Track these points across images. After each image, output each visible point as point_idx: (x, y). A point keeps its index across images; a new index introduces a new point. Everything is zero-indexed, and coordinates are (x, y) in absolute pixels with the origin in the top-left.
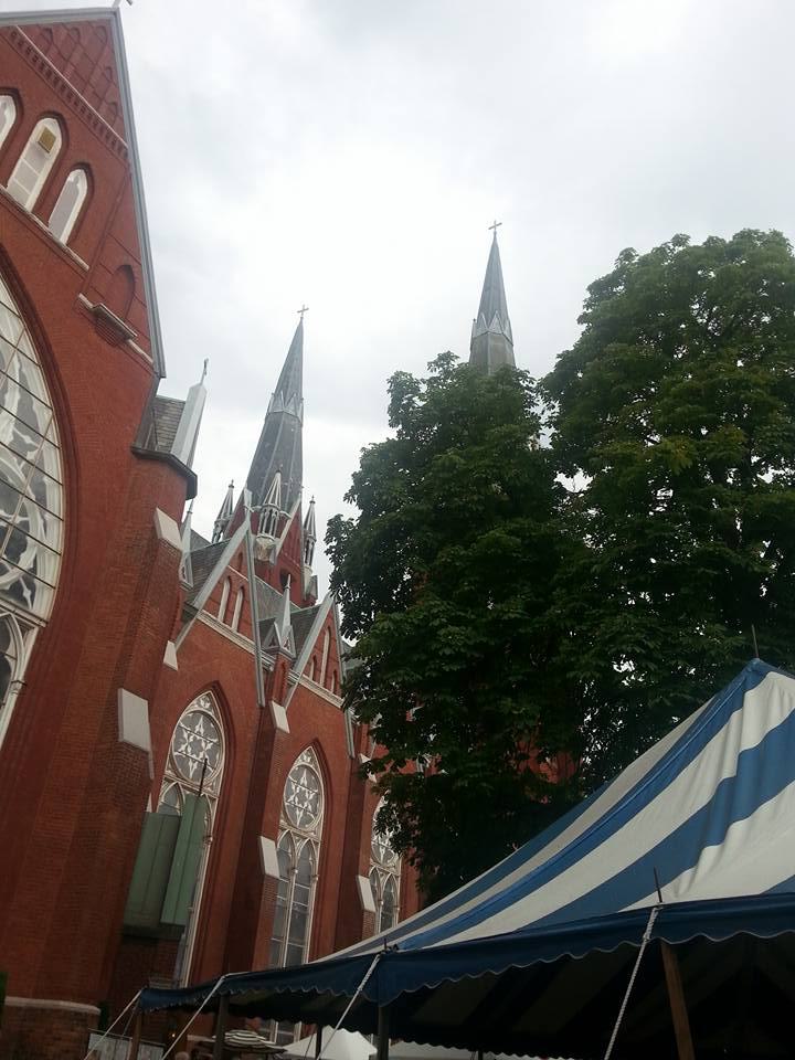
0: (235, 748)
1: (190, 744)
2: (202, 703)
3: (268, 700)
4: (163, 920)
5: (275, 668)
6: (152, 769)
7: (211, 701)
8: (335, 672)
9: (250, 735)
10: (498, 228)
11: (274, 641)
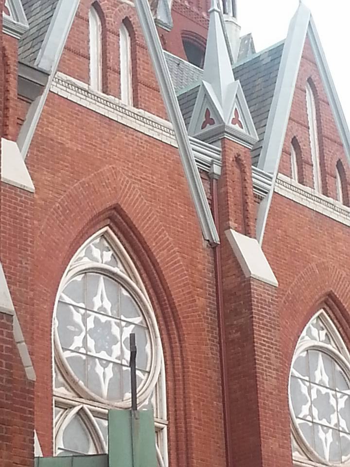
0: (178, 328)
1: (90, 332)
2: (96, 253)
3: (222, 228)
5: (223, 166)
6: (26, 359)
7: (112, 246)
8: (339, 165)
9: (201, 302)
11: (210, 116)
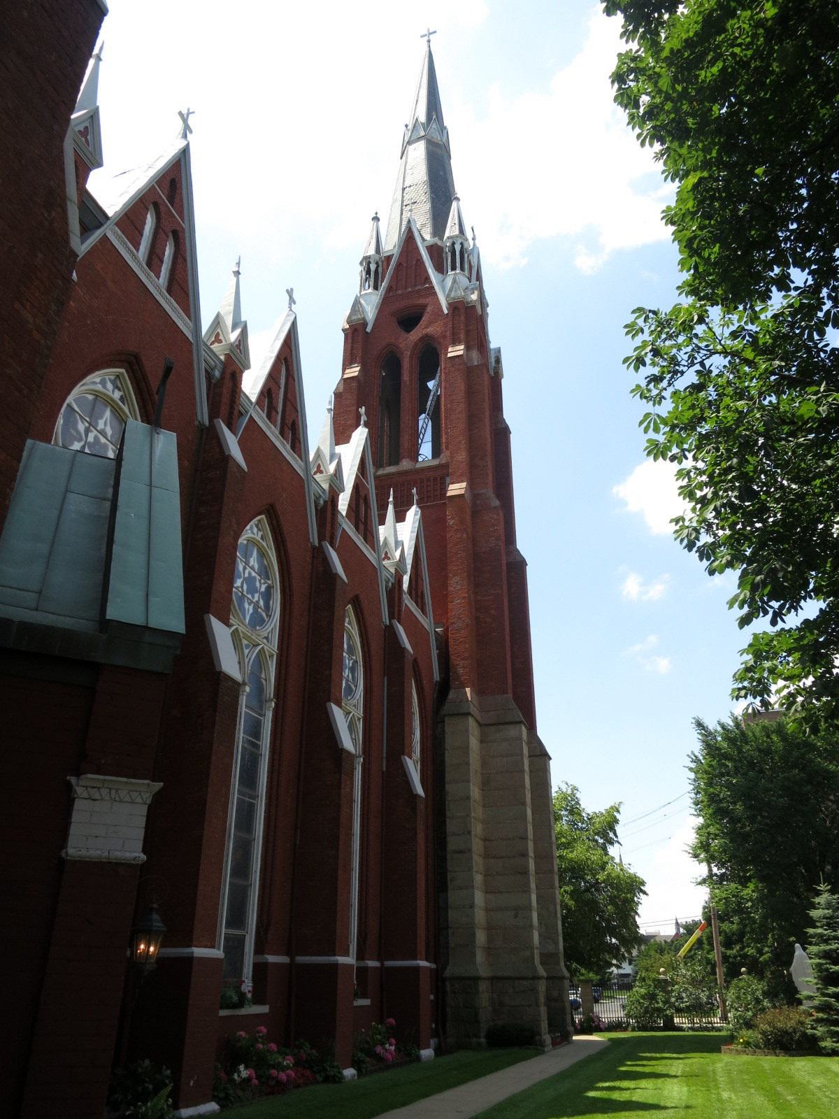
4: (112, 613)
10: (432, 37)
